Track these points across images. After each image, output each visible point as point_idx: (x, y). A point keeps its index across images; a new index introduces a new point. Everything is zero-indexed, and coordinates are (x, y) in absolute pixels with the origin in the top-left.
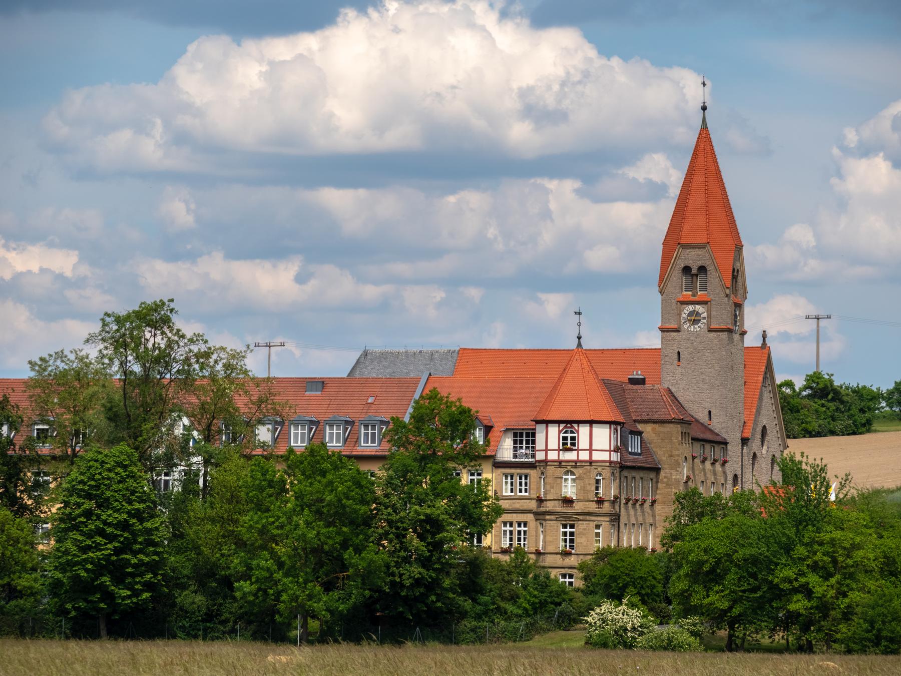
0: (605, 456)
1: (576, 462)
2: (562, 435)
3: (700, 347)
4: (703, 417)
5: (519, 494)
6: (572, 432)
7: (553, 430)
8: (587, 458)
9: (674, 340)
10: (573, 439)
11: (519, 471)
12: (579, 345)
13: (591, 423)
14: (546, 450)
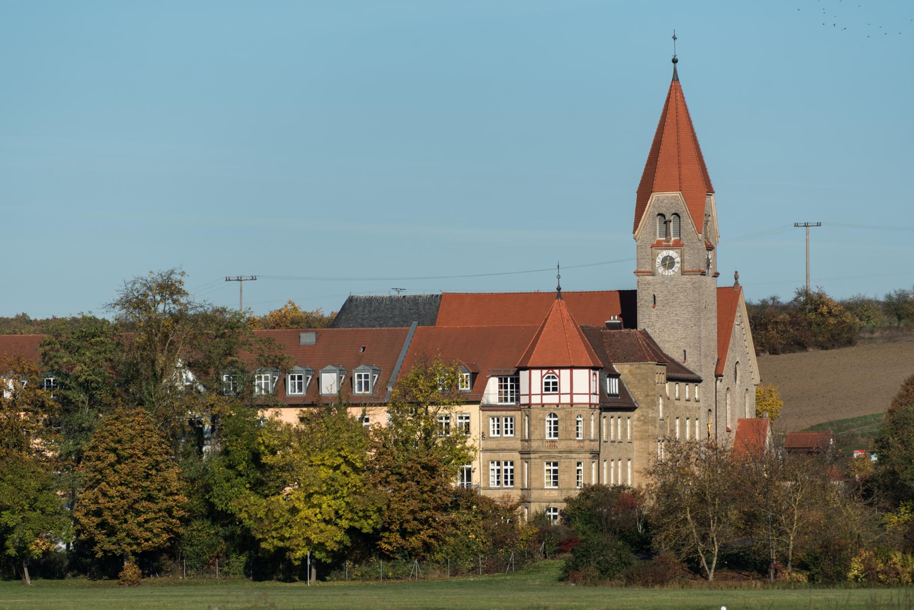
0: (585, 399)
1: (558, 405)
2: (544, 380)
3: (675, 290)
4: (677, 356)
6: (553, 377)
7: (536, 374)
8: (569, 401)
9: (649, 284)
13: (572, 368)
14: (530, 395)
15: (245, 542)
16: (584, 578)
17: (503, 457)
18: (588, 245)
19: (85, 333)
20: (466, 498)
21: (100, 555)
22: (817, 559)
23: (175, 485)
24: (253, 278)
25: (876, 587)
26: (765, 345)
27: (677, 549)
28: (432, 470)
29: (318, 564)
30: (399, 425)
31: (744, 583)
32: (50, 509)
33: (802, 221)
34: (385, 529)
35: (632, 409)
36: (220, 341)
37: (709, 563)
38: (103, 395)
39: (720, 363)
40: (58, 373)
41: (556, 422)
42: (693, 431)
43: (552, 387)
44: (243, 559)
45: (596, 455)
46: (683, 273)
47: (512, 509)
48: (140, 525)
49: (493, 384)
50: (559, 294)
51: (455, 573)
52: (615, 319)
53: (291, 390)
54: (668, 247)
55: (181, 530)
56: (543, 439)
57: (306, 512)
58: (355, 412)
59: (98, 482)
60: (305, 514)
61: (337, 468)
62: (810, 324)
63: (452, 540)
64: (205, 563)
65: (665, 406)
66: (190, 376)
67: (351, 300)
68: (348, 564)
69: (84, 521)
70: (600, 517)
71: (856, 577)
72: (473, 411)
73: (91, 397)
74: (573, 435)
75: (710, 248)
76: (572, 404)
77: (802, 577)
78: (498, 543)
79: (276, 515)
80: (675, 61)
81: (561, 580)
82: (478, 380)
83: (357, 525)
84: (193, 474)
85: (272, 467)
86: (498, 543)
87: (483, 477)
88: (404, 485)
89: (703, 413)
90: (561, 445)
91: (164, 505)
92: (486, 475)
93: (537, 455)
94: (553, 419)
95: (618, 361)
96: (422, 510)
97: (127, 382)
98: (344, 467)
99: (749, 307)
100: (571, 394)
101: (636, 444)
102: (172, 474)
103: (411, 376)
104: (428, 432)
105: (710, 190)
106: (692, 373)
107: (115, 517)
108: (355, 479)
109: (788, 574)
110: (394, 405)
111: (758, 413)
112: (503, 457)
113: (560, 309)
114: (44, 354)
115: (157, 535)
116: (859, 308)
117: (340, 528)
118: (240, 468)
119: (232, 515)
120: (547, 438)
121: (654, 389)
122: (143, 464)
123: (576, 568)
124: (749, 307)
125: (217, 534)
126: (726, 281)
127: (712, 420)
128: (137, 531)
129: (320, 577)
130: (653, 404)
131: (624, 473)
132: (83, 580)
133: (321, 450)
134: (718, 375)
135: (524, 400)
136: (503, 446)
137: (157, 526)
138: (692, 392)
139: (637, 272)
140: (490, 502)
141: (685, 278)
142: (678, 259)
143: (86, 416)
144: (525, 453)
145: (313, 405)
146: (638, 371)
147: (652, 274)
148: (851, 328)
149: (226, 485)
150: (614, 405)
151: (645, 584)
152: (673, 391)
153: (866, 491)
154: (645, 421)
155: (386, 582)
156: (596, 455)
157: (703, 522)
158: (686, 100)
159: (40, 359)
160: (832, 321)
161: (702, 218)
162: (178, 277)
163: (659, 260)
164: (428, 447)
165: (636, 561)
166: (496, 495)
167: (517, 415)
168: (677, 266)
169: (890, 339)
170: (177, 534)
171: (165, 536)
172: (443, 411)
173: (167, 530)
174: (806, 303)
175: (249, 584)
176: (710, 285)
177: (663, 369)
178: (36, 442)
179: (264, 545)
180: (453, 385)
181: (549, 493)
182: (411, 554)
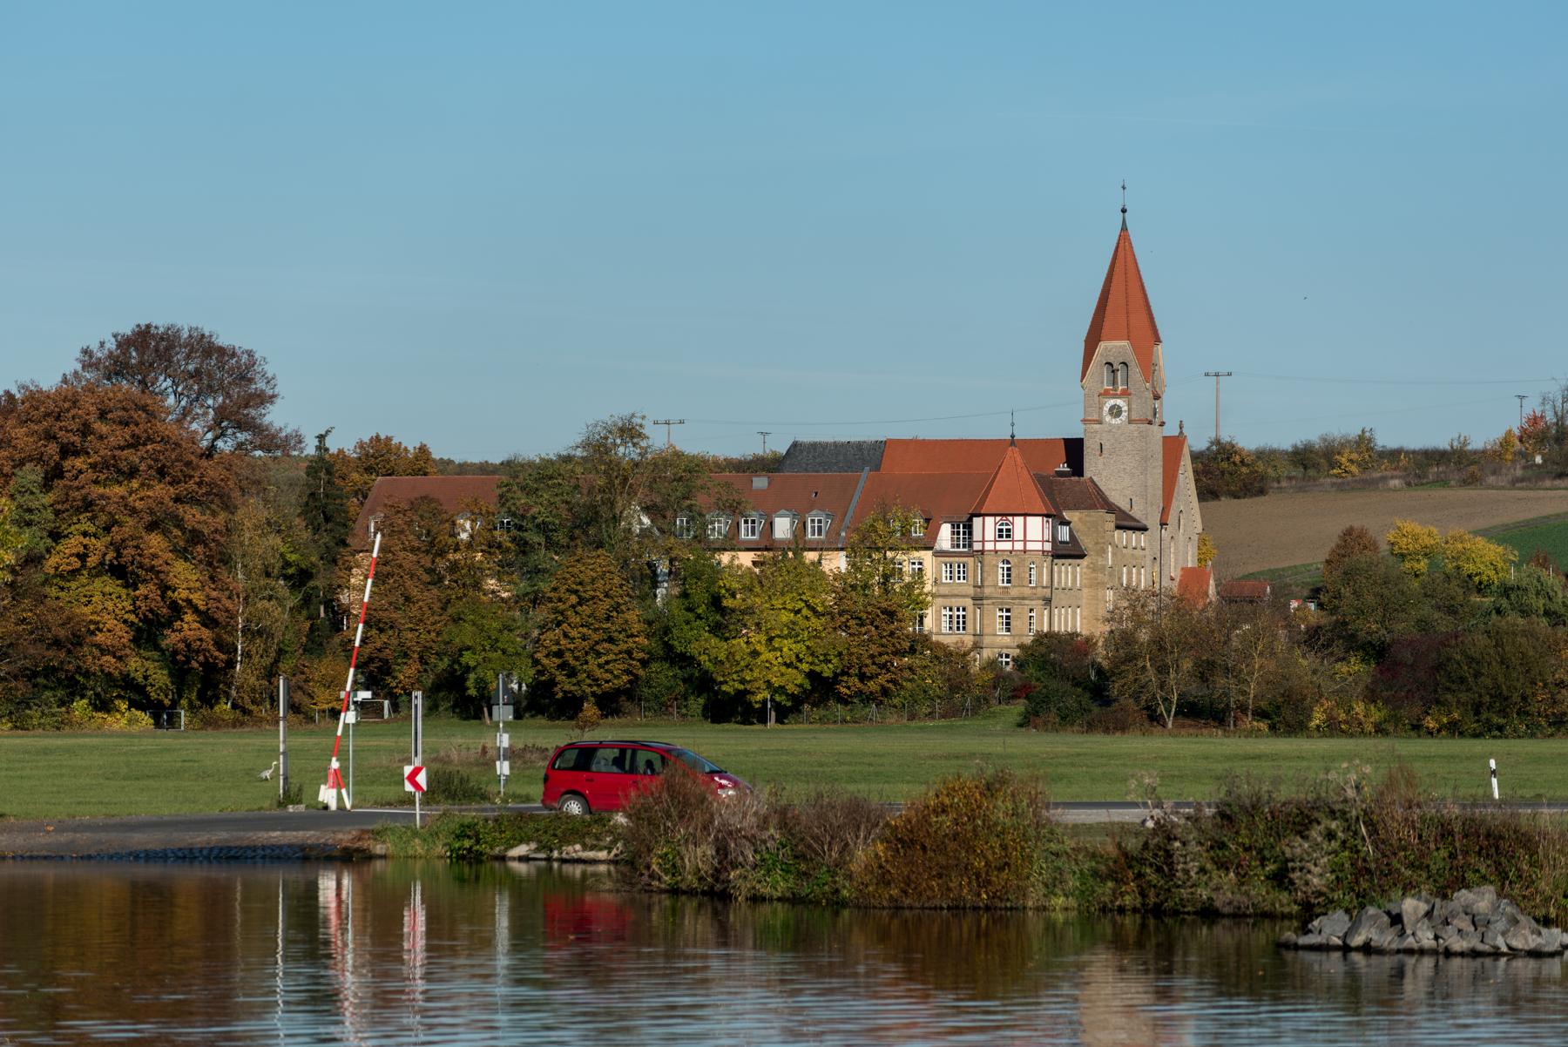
0: (1038, 546)
4: (1124, 506)
7: (990, 521)
13: (1025, 515)
14: (983, 541)
15: (703, 683)
16: (1045, 723)
17: (955, 602)
18: (1030, 390)
19: (544, 475)
20: (920, 643)
21: (560, 695)
22: (1278, 707)
23: (636, 628)
24: (681, 422)
25: (1339, 737)
26: (1207, 493)
27: (1136, 697)
28: (891, 615)
29: (778, 707)
30: (859, 569)
31: (1205, 731)
32: (511, 650)
33: (1212, 370)
34: (844, 673)
35: (1082, 556)
36: (681, 485)
37: (1169, 712)
38: (561, 537)
39: (1165, 511)
40: (514, 515)
42: (1142, 580)
43: (1005, 534)
44: (701, 701)
45: (1048, 601)
46: (1130, 421)
47: (965, 655)
48: (600, 666)
49: (946, 530)
50: (1013, 441)
51: (912, 717)
52: (1064, 468)
53: (744, 534)
54: (1115, 396)
55: (641, 672)
56: (996, 586)
57: (767, 655)
58: (811, 556)
59: (559, 624)
60: (768, 659)
61: (798, 612)
62: (1223, 473)
63: (908, 685)
64: (663, 704)
65: (1114, 554)
66: (646, 520)
67: (795, 445)
68: (806, 707)
69: (545, 661)
70: (1053, 664)
71: (1318, 727)
72: (927, 556)
73: (547, 538)
74: (1026, 582)
75: (1157, 397)
77: (1263, 726)
78: (954, 688)
79: (737, 658)
80: (1124, 211)
81: (1020, 725)
82: (931, 526)
83: (818, 669)
84: (651, 617)
85: (733, 611)
86: (954, 688)
87: (935, 623)
88: (863, 630)
89: (1148, 561)
90: (1014, 592)
91: (625, 647)
92: (938, 620)
95: (1069, 508)
96: (881, 654)
97: (588, 524)
98: (805, 612)
99: (1196, 457)
100: (1025, 541)
101: (1085, 590)
102: (632, 616)
103: (869, 521)
104: (886, 577)
105: (1158, 340)
106: (1134, 520)
107: (576, 658)
108: (816, 623)
109: (1248, 722)
110: (852, 550)
111: (1200, 560)
112: (955, 602)
113: (1013, 455)
114: (501, 496)
115: (617, 677)
116: (1266, 455)
117: (801, 671)
118: (700, 611)
119: (692, 658)
122: (605, 605)
123: (1037, 714)
124: (1196, 457)
125: (675, 676)
126: (1171, 430)
127: (1157, 569)
128: (598, 673)
129: (779, 720)
130: (1104, 551)
131: (1072, 620)
132: (541, 720)
133: (783, 594)
134: (1163, 524)
135: (977, 546)
137: (617, 668)
138: (1138, 541)
139: (1084, 421)
140: (939, 645)
141: (1133, 427)
142: (1125, 408)
143: (542, 557)
144: (978, 600)
145: (767, 549)
147: (1100, 422)
148: (1263, 478)
149: (686, 627)
150: (1066, 552)
151: (1107, 731)
152: (1121, 539)
153: (1313, 639)
154: (1094, 568)
155: (845, 726)
156: (1048, 601)
157: (1162, 670)
159: (496, 500)
160: (1244, 470)
161: (1149, 367)
162: (639, 421)
163: (1106, 409)
164: (887, 591)
165: (1096, 710)
166: (949, 640)
167: (970, 561)
168: (1125, 414)
169: (1301, 489)
170: (636, 676)
171: (625, 678)
172: (900, 557)
173: (628, 672)
174: (1218, 452)
175: (708, 725)
176: (1157, 433)
177: (1112, 517)
178: (491, 583)
179: (724, 688)
180: (905, 533)
181: (1001, 640)
182: (868, 698)
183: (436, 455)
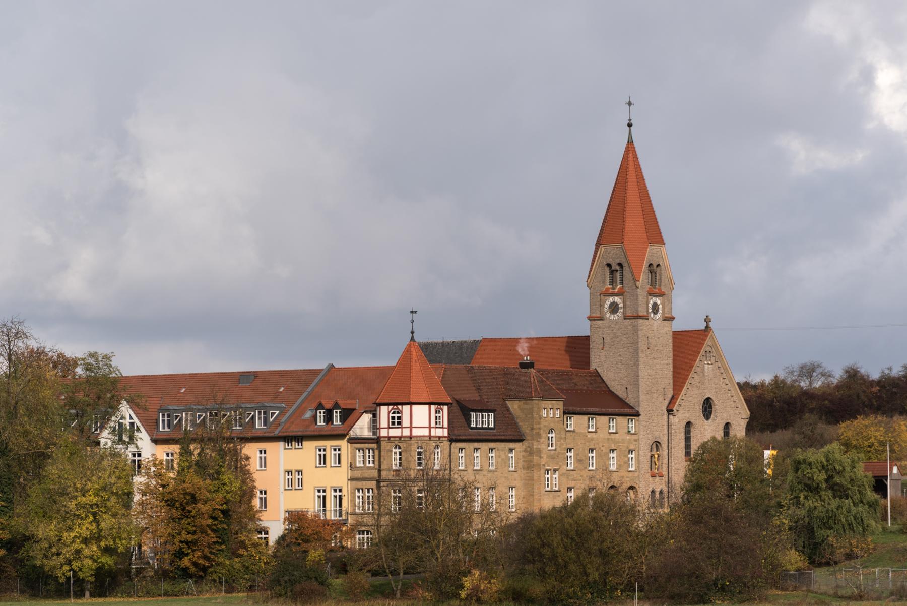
1: (400, 437)
2: (391, 415)
3: (619, 333)
5: (368, 465)
6: (398, 413)
8: (408, 434)
9: (599, 327)
10: (399, 418)
11: (367, 445)
12: (412, 339)
13: (411, 404)
41: (400, 453)
43: (397, 422)
54: (613, 295)
76: (430, 437)
80: (630, 125)
93: (385, 484)
94: (398, 451)
106: (633, 408)
120: (394, 468)
121: (539, 423)
136: (366, 475)
141: (627, 322)
146: (525, 406)
158: (640, 160)
183: (336, 366)
